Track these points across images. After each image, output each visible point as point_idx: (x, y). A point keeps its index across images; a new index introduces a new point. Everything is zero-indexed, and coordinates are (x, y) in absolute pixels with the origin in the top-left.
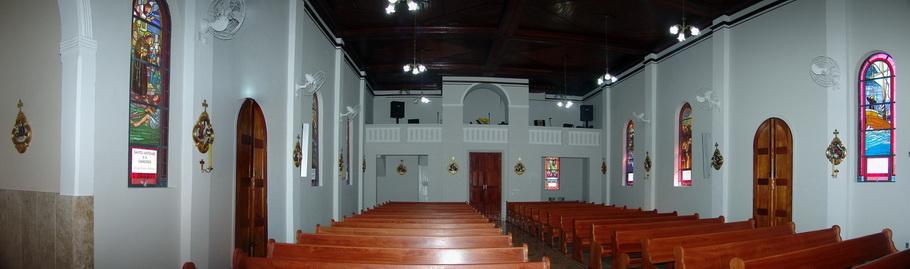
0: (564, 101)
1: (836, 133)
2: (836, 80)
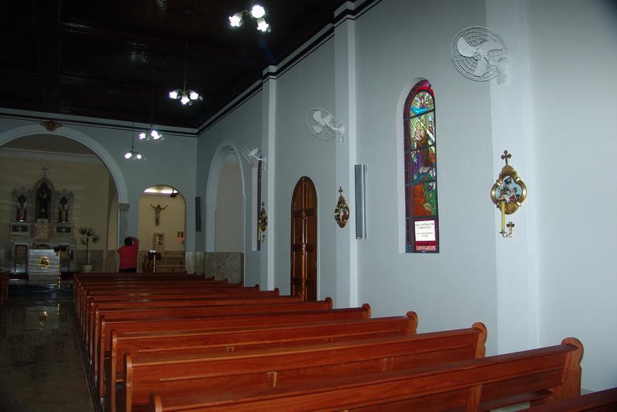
1: (506, 156)
2: (502, 83)
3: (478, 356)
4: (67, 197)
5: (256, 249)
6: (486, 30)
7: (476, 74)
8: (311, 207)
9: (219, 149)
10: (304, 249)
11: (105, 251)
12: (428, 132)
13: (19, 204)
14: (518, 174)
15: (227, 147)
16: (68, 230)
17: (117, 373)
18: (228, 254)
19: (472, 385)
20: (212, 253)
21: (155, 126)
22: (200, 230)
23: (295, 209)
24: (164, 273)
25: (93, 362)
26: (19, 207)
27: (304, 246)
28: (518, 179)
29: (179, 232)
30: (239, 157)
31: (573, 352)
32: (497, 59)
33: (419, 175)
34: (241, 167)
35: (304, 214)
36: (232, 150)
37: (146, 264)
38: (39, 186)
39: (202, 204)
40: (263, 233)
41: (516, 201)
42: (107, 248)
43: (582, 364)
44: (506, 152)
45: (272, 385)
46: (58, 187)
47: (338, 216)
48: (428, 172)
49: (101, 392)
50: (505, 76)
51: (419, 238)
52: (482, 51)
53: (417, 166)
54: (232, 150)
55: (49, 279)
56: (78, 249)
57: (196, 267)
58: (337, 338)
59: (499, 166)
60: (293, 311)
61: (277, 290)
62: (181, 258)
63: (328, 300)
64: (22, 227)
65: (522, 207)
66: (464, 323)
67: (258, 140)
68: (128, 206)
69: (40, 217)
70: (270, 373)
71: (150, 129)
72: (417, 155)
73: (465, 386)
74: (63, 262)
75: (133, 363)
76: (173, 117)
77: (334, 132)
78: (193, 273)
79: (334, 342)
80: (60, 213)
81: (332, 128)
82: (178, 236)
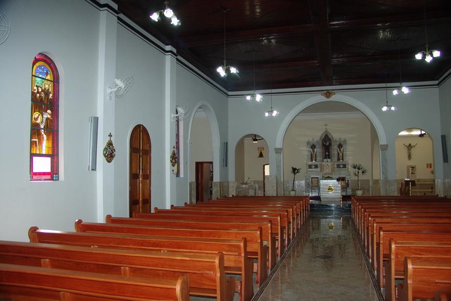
0: (399, 88)
16: (345, 166)
17: (395, 271)
21: (403, 84)
29: (427, 164)
42: (372, 178)
46: (336, 136)
49: (381, 284)
55: (332, 200)
56: (352, 179)
64: (314, 165)
68: (387, 146)
69: (325, 157)
71: (400, 87)
74: (344, 188)
75: (413, 265)
80: (338, 154)
82: (428, 167)
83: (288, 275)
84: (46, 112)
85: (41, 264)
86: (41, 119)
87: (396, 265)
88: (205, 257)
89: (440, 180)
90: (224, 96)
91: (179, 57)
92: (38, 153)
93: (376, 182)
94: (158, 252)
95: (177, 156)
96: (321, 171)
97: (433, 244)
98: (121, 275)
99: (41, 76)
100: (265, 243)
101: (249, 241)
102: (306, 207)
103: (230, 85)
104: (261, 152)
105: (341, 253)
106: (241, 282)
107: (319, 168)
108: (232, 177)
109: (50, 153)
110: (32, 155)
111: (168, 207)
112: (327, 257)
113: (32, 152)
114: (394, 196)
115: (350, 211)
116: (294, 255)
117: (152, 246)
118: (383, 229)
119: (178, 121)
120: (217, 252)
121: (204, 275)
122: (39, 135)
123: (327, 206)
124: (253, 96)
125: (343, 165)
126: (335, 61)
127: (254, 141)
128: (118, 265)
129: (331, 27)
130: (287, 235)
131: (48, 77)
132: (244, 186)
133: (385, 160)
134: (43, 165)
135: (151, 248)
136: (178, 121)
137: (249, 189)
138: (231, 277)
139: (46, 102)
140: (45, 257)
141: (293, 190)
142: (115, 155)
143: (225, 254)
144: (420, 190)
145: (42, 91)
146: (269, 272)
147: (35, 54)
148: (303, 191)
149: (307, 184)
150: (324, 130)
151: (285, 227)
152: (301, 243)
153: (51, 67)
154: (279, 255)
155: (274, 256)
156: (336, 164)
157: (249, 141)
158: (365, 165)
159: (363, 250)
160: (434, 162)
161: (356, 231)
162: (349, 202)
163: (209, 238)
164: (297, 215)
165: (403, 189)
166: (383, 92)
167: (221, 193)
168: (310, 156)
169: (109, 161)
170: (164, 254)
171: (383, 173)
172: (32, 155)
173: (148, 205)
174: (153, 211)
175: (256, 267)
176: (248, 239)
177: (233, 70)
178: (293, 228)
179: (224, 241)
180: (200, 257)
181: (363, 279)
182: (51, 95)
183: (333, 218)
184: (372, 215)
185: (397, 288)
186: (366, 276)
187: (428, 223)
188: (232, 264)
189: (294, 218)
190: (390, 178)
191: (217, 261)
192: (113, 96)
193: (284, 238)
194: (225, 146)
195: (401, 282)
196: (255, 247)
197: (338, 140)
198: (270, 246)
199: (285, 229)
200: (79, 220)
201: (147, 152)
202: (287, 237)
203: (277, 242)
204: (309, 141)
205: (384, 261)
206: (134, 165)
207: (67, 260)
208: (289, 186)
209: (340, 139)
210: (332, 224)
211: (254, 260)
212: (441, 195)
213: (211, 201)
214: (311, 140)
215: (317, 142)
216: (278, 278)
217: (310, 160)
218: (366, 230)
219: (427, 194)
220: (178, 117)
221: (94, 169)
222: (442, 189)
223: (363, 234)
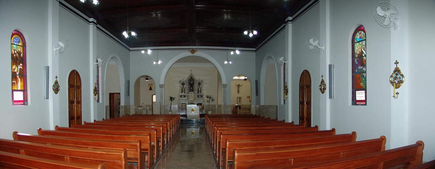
0: (234, 51)
1: (397, 63)
3: (382, 150)
4: (201, 82)
5: (283, 104)
6: (390, 4)
7: (385, 24)
8: (308, 84)
9: (265, 57)
10: (305, 104)
11: (216, 105)
12: (363, 50)
13: (182, 86)
14: (401, 71)
15: (269, 56)
16: (202, 96)
17: (228, 157)
18: (270, 106)
19: (380, 162)
20: (264, 105)
21: (237, 48)
22: (258, 95)
23: (301, 85)
24: (242, 115)
25: (216, 152)
26: (182, 87)
27: (305, 102)
28: (401, 73)
29: (248, 96)
30: (275, 61)
31: (420, 147)
32: (394, 18)
33: (358, 70)
34: (276, 66)
35: (305, 87)
36: (272, 58)
37: (234, 110)
38: (189, 78)
39: (258, 85)
40: (286, 96)
41: (400, 83)
42: (217, 104)
43: (423, 151)
44: (396, 61)
45: (291, 164)
46: (197, 78)
47: (321, 88)
48: (362, 68)
49: (220, 165)
50: (397, 26)
51: (358, 99)
52: (388, 13)
53: (358, 66)
54: (272, 58)
55: (194, 117)
56: (206, 104)
57: (256, 112)
58: (320, 144)
59: (394, 67)
60: (300, 132)
61: (293, 122)
62: (249, 108)
63: (316, 127)
64: (184, 96)
65: (403, 85)
66: (376, 136)
67: (284, 53)
68: (226, 85)
69: (190, 91)
70: (290, 159)
71: (235, 50)
72: (357, 60)
73: (376, 163)
74: (201, 110)
75: (238, 153)
76: (245, 44)
77: (319, 49)
78: (255, 114)
79: (319, 145)
80: (198, 89)
81: (318, 47)
82: (248, 98)
83: (167, 163)
84: (20, 65)
85: (20, 152)
86: (17, 69)
87: (229, 154)
88: (115, 152)
89: (254, 105)
90: (127, 51)
91: (98, 26)
92: (16, 89)
93: (220, 106)
94: (86, 148)
95: (97, 89)
96: (188, 99)
97: (248, 141)
98: (65, 161)
99: (16, 44)
100: (153, 143)
101: (143, 142)
102: (178, 122)
103: (131, 43)
104: (151, 87)
105: (198, 149)
106: (138, 167)
107: (186, 98)
108: (132, 103)
109: (23, 89)
110: (13, 91)
111: (92, 121)
112: (190, 151)
113: (13, 89)
114: (229, 115)
115: (204, 123)
116: (170, 150)
117: (83, 145)
118: (222, 133)
119: (98, 67)
120: (123, 149)
121: (115, 163)
122: (16, 78)
123: (190, 120)
124: (146, 51)
125: (201, 96)
126: (198, 30)
127: (146, 80)
128: (62, 155)
129: (196, 8)
130: (166, 139)
131: (20, 44)
132: (140, 108)
133: (225, 93)
134: (19, 96)
135: (82, 146)
136: (98, 67)
137: (143, 110)
138: (131, 164)
139: (19, 59)
140: (22, 149)
141: (170, 111)
142: (59, 89)
143: (128, 150)
144: (243, 111)
145: (17, 52)
146: (155, 161)
147: (12, 31)
148: (176, 112)
149: (179, 107)
150: (190, 74)
151: (165, 133)
152: (175, 143)
153: (20, 36)
154: (161, 150)
155: (158, 151)
156: (196, 95)
157: (143, 80)
158: (214, 96)
159: (211, 146)
160: (251, 95)
161: (207, 135)
162: (204, 118)
163: (118, 140)
164: (173, 126)
165: (234, 110)
166: (225, 52)
167: (125, 113)
168: (181, 90)
169: (56, 93)
170: (90, 150)
171: (224, 101)
172: (13, 91)
173: (80, 120)
174: (83, 124)
175: (147, 158)
176: (142, 141)
177: (133, 34)
178: (170, 134)
179: (127, 142)
180: (113, 152)
181: (210, 163)
182: (22, 54)
183: (194, 128)
184: (216, 126)
185: (229, 167)
186: (212, 161)
187: (247, 130)
188: (132, 156)
189: (170, 128)
190: (228, 104)
191: (123, 154)
192: (58, 52)
193: (164, 140)
194: (128, 83)
195: (231, 163)
196: (146, 146)
197: (198, 80)
198: (156, 146)
199: (165, 134)
200: (40, 128)
201: (79, 87)
202: (166, 139)
203: (160, 143)
204: (180, 80)
205: (222, 152)
206: (71, 95)
207: (34, 151)
208: (168, 108)
209: (199, 79)
210: (194, 131)
211: (146, 154)
212: (254, 114)
213: (119, 117)
214: (182, 79)
215: (186, 81)
216: (160, 164)
217: (181, 92)
218: (213, 134)
219: (247, 113)
220: (98, 65)
221: (47, 98)
222: (255, 111)
223: (211, 137)
